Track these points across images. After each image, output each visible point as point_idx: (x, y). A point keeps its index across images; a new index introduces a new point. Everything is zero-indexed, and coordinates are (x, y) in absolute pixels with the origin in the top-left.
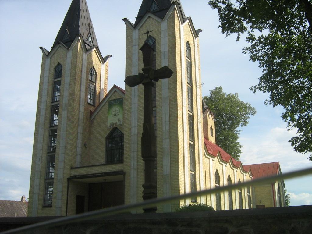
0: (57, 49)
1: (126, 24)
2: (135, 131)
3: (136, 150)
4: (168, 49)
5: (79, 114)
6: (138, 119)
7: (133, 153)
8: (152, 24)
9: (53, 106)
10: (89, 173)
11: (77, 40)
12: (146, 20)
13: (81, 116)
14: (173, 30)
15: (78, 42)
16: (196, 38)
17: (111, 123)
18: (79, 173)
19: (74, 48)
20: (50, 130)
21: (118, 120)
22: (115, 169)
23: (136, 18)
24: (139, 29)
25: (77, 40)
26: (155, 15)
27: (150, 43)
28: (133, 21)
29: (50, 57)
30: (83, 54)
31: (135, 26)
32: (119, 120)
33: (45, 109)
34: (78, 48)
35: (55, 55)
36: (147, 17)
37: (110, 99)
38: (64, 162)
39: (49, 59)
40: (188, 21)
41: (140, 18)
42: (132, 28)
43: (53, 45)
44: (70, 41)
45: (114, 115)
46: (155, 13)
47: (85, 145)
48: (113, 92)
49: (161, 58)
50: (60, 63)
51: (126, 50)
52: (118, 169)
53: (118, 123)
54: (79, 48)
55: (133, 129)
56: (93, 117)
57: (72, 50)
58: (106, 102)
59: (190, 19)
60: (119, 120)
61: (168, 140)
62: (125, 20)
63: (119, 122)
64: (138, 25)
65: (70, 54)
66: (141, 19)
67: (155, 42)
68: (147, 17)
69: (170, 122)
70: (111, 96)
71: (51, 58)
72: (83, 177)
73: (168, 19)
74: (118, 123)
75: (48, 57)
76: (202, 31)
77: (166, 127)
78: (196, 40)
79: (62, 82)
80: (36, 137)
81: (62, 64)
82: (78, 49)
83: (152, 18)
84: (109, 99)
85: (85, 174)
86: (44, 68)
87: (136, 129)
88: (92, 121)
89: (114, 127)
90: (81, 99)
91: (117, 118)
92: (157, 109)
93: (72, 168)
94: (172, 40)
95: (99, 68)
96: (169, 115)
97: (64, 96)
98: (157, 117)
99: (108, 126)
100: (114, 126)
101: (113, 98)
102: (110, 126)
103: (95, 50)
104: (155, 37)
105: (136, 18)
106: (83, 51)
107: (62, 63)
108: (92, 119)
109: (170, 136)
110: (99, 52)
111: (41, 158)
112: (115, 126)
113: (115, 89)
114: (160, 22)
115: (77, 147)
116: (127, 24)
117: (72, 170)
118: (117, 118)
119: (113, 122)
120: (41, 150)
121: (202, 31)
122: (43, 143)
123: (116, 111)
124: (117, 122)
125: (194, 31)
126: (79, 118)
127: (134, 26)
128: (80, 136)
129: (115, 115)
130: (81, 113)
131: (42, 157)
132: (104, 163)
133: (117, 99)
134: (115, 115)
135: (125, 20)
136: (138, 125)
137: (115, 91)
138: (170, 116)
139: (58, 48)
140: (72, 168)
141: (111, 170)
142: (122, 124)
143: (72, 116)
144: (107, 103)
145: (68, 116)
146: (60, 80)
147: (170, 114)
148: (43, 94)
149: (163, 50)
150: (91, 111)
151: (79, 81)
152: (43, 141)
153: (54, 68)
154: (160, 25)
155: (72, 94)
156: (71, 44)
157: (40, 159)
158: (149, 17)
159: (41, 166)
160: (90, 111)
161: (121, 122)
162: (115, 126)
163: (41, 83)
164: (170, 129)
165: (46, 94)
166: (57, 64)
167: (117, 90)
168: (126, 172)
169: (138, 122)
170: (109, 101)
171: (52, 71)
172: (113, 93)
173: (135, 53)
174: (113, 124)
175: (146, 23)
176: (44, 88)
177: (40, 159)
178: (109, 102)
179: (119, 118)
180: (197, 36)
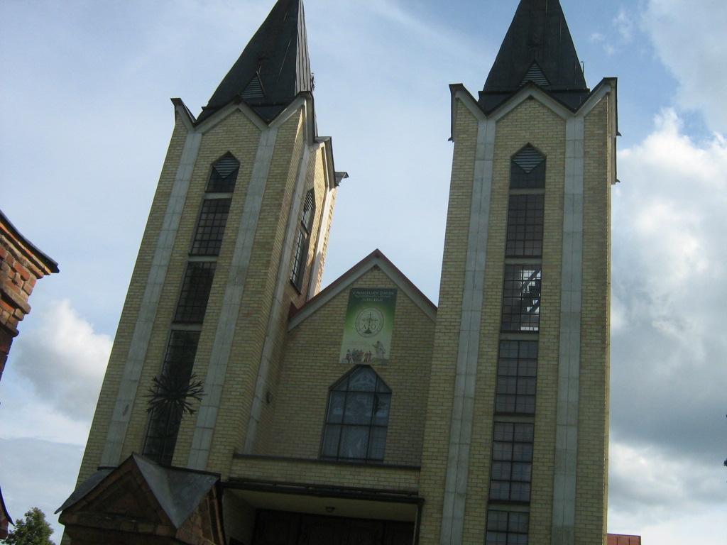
0: (229, 116)
1: (176, 113)
2: (467, 385)
3: (468, 441)
4: (584, 191)
5: (272, 304)
6: (480, 356)
7: (457, 446)
8: (538, 117)
9: (190, 264)
10: (297, 481)
11: (299, 106)
12: (520, 105)
13: (276, 315)
14: (599, 146)
15: (299, 111)
16: (331, 188)
17: (351, 351)
18: (258, 474)
19: (284, 124)
20: (172, 331)
21: (376, 347)
22: (386, 484)
23: (202, 108)
24: (497, 122)
25: (299, 106)
26: (554, 98)
27: (528, 164)
28: (196, 112)
29: (203, 128)
30: (303, 148)
31: (196, 124)
32: (378, 346)
33: (166, 268)
34: (297, 127)
35: (219, 130)
36: (526, 95)
37: (356, 286)
38: (213, 434)
39: (198, 136)
40: (322, 145)
41: (211, 110)
42: (189, 126)
43: (207, 103)
44: (504, 93)
45: (364, 330)
46: (253, 107)
47: (268, 398)
48: (370, 266)
49: (562, 208)
50: (233, 153)
51: (454, 164)
52: (407, 485)
53: (374, 356)
54: (299, 126)
55: (461, 381)
56: (296, 322)
57: (279, 128)
58: (344, 290)
59: (329, 142)
60: (378, 346)
61: (573, 432)
62: (177, 102)
63: (377, 352)
64: (207, 120)
65: (270, 136)
66: (212, 113)
67: (236, 172)
68: (526, 95)
69: (580, 381)
70: (360, 277)
71: (203, 134)
72: (274, 487)
73: (587, 115)
74: (374, 356)
75: (195, 130)
76: (347, 176)
77: (569, 394)
78: (330, 194)
79: (233, 205)
80: (120, 340)
81: (239, 159)
82: (298, 131)
83: (538, 101)
84: (352, 283)
85: (283, 480)
86: (179, 156)
87: (472, 380)
88: (289, 332)
89: (358, 363)
90: (284, 265)
91: (372, 341)
92: (541, 340)
93: (236, 456)
94: (596, 171)
95: (321, 198)
96: (581, 362)
97: (239, 245)
98: (541, 362)
99: (343, 356)
100: (360, 360)
101: (367, 283)
102: (348, 358)
103: (322, 148)
104: (544, 151)
105: (202, 108)
106: (304, 140)
107: (238, 155)
108: (290, 328)
109: (579, 421)
110: (330, 153)
111: (130, 408)
112: (363, 360)
113: (375, 262)
114: (261, 129)
115: (254, 395)
116: (180, 113)
117: (236, 461)
118: (372, 341)
119: (359, 348)
120: (136, 381)
121: (347, 176)
122: (145, 362)
123: (370, 320)
124: (373, 351)
125: (332, 174)
126: (269, 316)
127: (193, 122)
128: (265, 363)
129: (368, 332)
130: (277, 302)
131: (135, 405)
132: (316, 457)
133: (379, 290)
134: (368, 332)
135: (177, 102)
136: (479, 372)
137: (376, 267)
138: (581, 367)
139: (233, 113)
140: (236, 456)
141: (375, 483)
142: (384, 360)
143: (256, 305)
144: (346, 295)
145: (241, 303)
146: (230, 200)
147: (583, 360)
148: (165, 226)
149: (569, 189)
150: (292, 303)
151: (285, 214)
152: (146, 357)
153: (211, 164)
154: (259, 135)
155: (264, 245)
156: (280, 113)
157: (127, 407)
158: (531, 98)
159: (128, 430)
160: (290, 304)
161: (383, 353)
162: (363, 360)
163: (163, 194)
164: (580, 400)
165: (175, 226)
166: (222, 153)
167: (382, 266)
168: (426, 499)
169: (479, 364)
170: (353, 290)
171: (205, 170)
172: (368, 272)
173: (482, 180)
174: (357, 355)
175: (519, 110)
176: (169, 210)
177: (127, 407)
178: (351, 293)
179: (378, 342)
180: (336, 185)
